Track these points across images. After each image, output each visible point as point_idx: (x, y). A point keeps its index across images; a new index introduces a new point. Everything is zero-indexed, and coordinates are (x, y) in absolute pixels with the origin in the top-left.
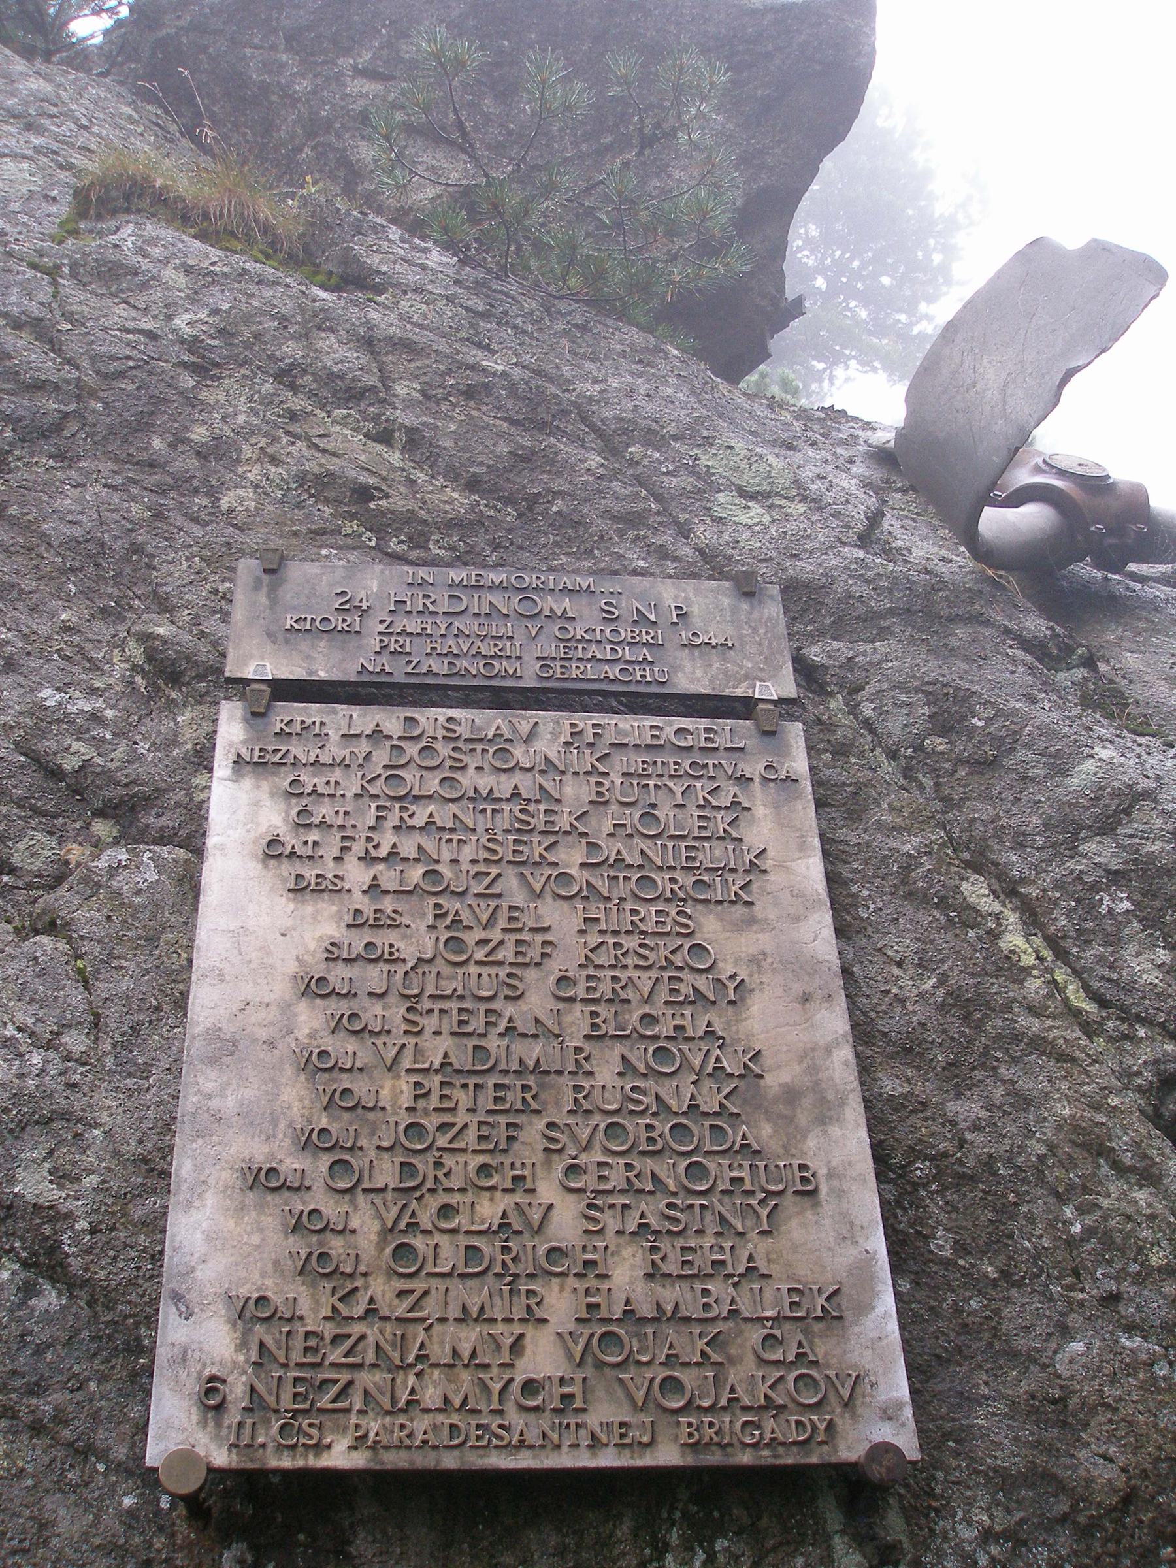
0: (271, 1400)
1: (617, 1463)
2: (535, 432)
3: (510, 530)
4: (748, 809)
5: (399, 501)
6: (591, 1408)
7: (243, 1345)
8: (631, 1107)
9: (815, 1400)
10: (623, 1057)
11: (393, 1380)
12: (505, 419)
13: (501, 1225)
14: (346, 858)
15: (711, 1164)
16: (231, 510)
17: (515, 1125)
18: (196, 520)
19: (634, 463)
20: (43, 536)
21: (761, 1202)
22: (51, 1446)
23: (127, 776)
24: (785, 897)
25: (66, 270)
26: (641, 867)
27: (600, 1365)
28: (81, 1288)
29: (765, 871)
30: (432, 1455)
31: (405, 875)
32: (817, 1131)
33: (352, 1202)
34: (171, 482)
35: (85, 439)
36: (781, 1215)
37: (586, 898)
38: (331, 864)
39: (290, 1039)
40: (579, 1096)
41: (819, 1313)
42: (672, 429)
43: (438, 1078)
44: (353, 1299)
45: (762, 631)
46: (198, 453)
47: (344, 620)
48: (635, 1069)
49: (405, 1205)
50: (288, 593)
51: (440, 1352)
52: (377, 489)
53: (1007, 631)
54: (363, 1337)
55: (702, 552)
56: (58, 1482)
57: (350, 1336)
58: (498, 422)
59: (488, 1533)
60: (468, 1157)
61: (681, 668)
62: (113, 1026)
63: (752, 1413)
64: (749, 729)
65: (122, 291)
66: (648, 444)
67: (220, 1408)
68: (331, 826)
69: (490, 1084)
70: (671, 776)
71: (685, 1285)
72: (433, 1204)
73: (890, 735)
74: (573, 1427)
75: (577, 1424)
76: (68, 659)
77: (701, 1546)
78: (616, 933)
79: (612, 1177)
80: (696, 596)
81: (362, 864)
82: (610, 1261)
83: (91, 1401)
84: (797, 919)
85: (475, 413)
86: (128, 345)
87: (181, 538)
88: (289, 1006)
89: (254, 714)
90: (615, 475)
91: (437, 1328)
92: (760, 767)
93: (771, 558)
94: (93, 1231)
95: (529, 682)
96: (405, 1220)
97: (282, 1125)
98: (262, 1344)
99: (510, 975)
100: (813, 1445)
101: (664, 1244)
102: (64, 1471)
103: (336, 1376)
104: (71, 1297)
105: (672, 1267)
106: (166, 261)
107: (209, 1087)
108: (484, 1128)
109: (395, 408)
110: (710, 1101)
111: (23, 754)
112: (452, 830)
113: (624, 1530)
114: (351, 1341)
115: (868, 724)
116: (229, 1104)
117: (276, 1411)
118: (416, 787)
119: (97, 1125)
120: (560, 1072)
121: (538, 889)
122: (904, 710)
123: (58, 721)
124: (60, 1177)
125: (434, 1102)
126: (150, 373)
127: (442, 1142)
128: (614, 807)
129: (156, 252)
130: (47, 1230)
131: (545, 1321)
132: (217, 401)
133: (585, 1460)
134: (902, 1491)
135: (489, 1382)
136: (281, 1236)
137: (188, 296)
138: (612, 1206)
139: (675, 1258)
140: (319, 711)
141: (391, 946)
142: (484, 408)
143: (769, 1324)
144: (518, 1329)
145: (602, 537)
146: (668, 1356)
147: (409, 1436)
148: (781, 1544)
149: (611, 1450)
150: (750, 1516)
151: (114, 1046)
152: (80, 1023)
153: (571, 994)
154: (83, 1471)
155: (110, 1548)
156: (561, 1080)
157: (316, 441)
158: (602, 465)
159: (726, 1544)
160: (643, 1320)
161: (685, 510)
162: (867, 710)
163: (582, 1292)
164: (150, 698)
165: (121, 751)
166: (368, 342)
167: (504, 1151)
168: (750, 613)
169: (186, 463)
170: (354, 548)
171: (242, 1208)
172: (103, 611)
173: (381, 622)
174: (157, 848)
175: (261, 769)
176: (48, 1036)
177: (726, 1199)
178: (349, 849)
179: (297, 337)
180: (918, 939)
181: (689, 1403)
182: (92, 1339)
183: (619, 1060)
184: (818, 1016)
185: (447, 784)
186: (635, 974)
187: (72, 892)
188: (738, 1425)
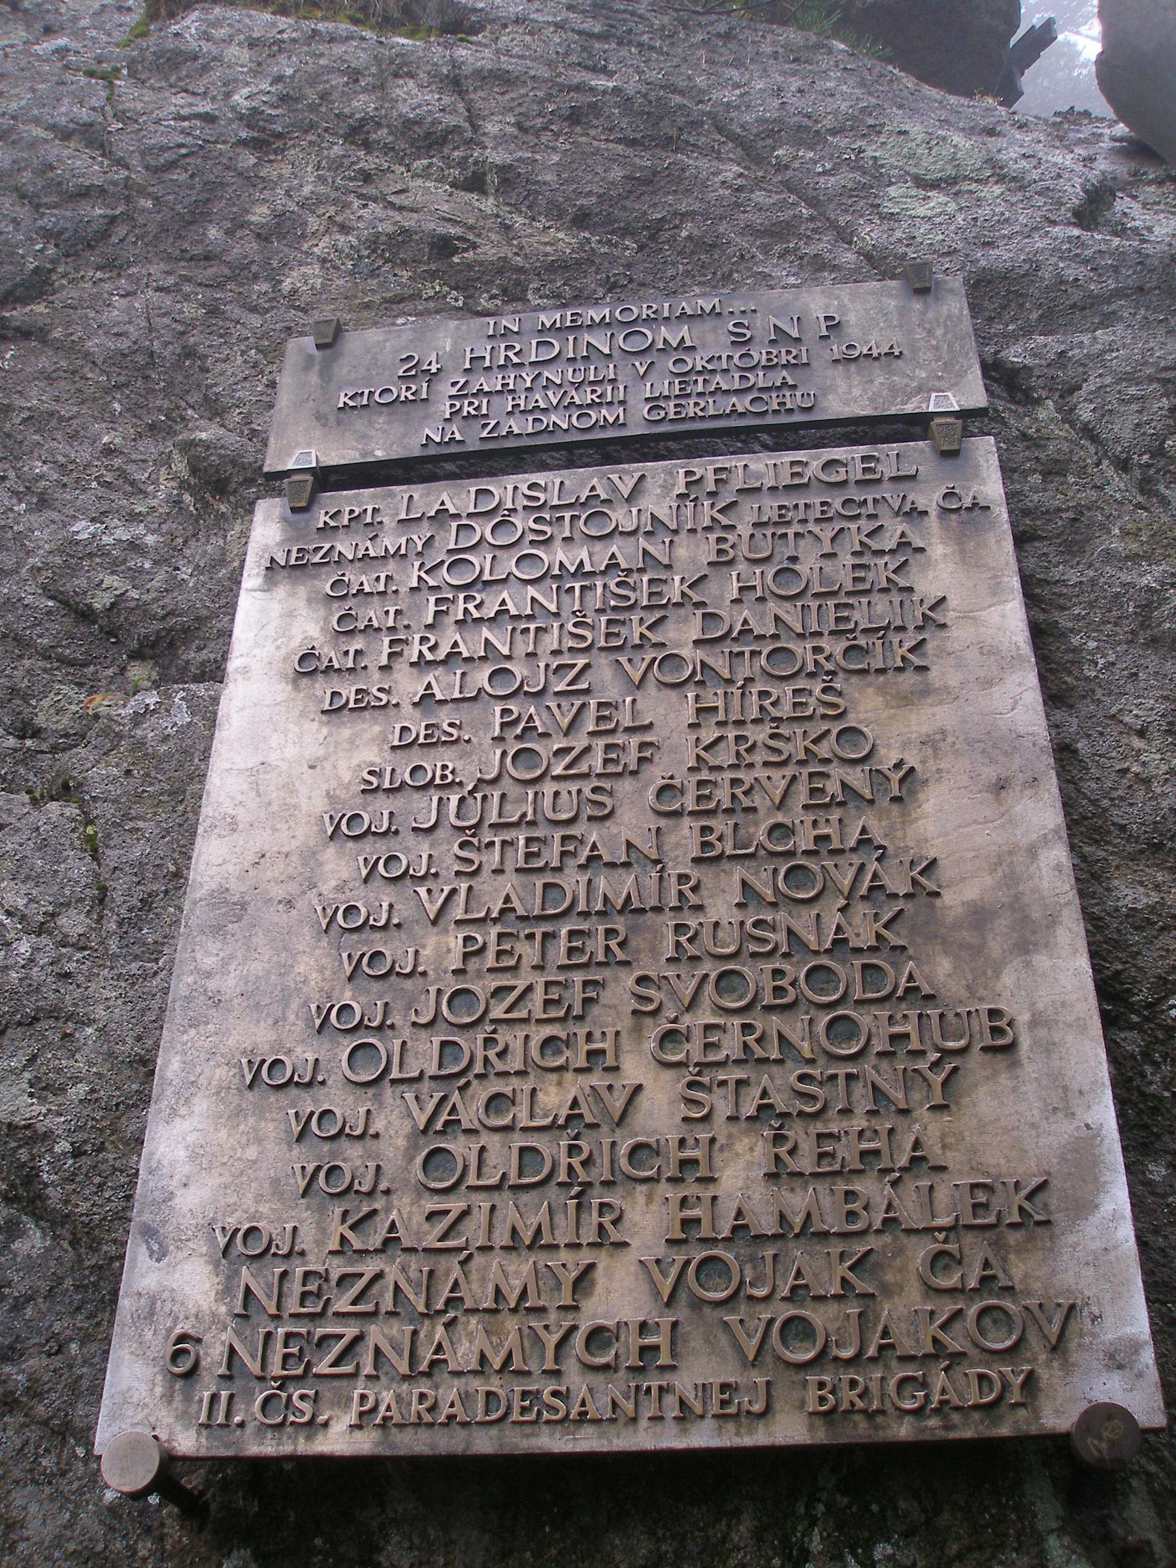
0: (255, 1367)
1: (715, 1443)
2: (658, 151)
3: (629, 266)
4: (921, 550)
5: (490, 250)
6: (682, 1364)
7: (226, 1291)
8: (753, 947)
9: (1008, 1343)
10: (744, 883)
11: (415, 1333)
12: (619, 141)
13: (569, 1118)
14: (396, 666)
15: (864, 1019)
16: (294, 292)
17: (595, 983)
18: (254, 309)
19: (781, 167)
20: (87, 354)
21: (935, 1065)
22: (25, 1425)
23: (163, 607)
24: (972, 656)
25: (125, 72)
26: (775, 637)
27: (698, 1304)
28: (63, 1225)
29: (944, 626)
30: (461, 1434)
31: (468, 678)
32: (1017, 963)
33: (377, 1098)
34: (227, 271)
35: (135, 243)
36: (964, 1081)
37: (701, 683)
38: (377, 675)
39: (312, 896)
40: (683, 939)
41: (1016, 1218)
42: (828, 122)
43: (494, 931)
44: (368, 1226)
45: (939, 332)
46: (259, 235)
47: (408, 389)
48: (760, 897)
49: (444, 1099)
50: (343, 369)
51: (479, 1293)
52: (460, 239)
54: (379, 1276)
55: (868, 257)
56: (31, 1471)
57: (361, 1275)
58: (611, 146)
59: (557, 1536)
60: (532, 1029)
61: (832, 389)
62: (119, 900)
63: (914, 1366)
64: (922, 451)
65: (180, 79)
66: (799, 143)
67: (191, 1374)
68: (379, 629)
69: (564, 932)
70: (817, 520)
71: (822, 1187)
72: (481, 1093)
73: (1117, 440)
74: (654, 1392)
75: (661, 1388)
76: (107, 485)
77: (855, 1555)
78: (740, 723)
79: (725, 1043)
81: (414, 671)
82: (718, 1158)
83: (71, 1367)
84: (988, 683)
85: (583, 139)
86: (182, 132)
87: (238, 331)
88: (314, 853)
89: (294, 510)
90: (758, 184)
91: (479, 1260)
92: (937, 496)
93: (955, 250)
94: (77, 1153)
95: (636, 429)
96: (444, 1117)
97: (295, 1004)
98: (248, 1291)
99: (595, 790)
100: (1003, 1408)
101: (795, 1132)
102: (37, 1456)
103: (339, 1330)
104: (55, 1237)
105: (805, 1163)
106: (229, 40)
107: (209, 962)
108: (554, 989)
109: (485, 148)
110: (862, 933)
111: (52, 598)
112: (531, 618)
113: (743, 1531)
114: (361, 1284)
115: (1088, 432)
116: (229, 984)
117: (261, 1379)
118: (487, 571)
119: (91, 1022)
120: (658, 910)
121: (636, 677)
122: (1134, 407)
123: (91, 555)
124: (42, 1089)
125: (490, 960)
126: (205, 158)
127: (498, 1012)
128: (742, 567)
129: (221, 33)
130: (23, 1155)
131: (625, 1244)
132: (280, 176)
133: (671, 1439)
134: (1152, 1468)
135: (542, 1333)
136: (285, 1147)
137: (251, 70)
138: (723, 1083)
139: (808, 1147)
140: (373, 497)
141: (444, 767)
142: (592, 132)
143: (941, 1236)
144: (585, 1257)
145: (742, 256)
146: (794, 1289)
147: (432, 1409)
148: (969, 1549)
149: (709, 1423)
150: (924, 1510)
151: (120, 924)
152: (81, 900)
153: (676, 806)
154: (59, 1457)
155: (86, 1555)
156: (659, 919)
157: (392, 198)
158: (741, 175)
159: (890, 1550)
160: (760, 1238)
161: (846, 211)
162: (1085, 413)
163: (675, 1204)
164: (199, 516)
165: (160, 578)
166: (454, 82)
167: (580, 1018)
168: (924, 313)
169: (246, 248)
170: (437, 312)
171: (238, 1113)
172: (152, 427)
173: (454, 384)
174: (193, 687)
175: (298, 573)
176: (40, 918)
177: (885, 1065)
178: (400, 654)
179: (370, 89)
180: (1166, 698)
181: (823, 1353)
182: (77, 1288)
183: (738, 887)
184: (1019, 808)
185: (525, 564)
186: (761, 773)
187: (90, 747)
188: (892, 1383)
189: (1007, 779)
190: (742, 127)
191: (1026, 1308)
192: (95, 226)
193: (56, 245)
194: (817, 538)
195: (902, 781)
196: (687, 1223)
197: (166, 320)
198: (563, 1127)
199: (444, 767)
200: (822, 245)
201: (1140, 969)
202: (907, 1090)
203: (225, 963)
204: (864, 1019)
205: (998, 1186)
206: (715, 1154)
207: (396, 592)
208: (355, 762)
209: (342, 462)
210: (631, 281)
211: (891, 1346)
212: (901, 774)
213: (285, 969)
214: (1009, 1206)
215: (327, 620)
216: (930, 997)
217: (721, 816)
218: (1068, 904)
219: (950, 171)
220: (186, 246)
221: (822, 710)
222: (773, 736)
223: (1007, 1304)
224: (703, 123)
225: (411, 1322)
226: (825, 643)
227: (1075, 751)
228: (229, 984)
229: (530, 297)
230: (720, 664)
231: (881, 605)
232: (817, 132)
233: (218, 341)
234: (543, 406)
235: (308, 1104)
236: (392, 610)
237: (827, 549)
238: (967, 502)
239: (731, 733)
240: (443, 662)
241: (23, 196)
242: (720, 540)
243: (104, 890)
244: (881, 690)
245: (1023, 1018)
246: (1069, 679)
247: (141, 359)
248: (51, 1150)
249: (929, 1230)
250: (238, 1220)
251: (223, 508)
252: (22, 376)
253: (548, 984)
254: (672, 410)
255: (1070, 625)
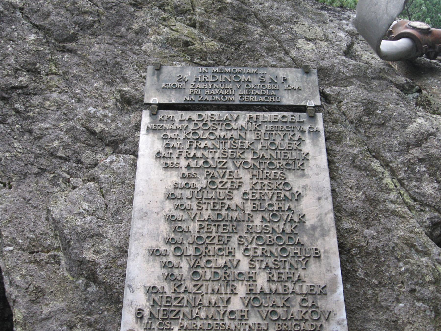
2: (241, 22)
3: (232, 54)
4: (304, 141)
5: (197, 46)
6: (250, 319)
7: (149, 300)
8: (265, 231)
10: (263, 217)
12: (231, 18)
13: (224, 266)
15: (289, 248)
18: (134, 53)
21: (303, 260)
24: (314, 168)
26: (270, 159)
27: (253, 307)
31: (198, 162)
32: (321, 238)
33: (181, 259)
36: (309, 263)
39: (163, 212)
40: (249, 228)
41: (319, 293)
42: (285, 19)
44: (180, 287)
45: (310, 84)
46: (135, 32)
48: (266, 220)
49: (196, 260)
50: (163, 76)
53: (391, 82)
54: (183, 298)
58: (229, 19)
61: (284, 97)
70: (280, 131)
73: (350, 116)
74: (244, 324)
76: (97, 98)
78: (262, 179)
80: (290, 73)
93: (315, 60)
94: (106, 268)
96: (196, 264)
97: (161, 237)
105: (275, 279)
107: (139, 226)
109: (196, 16)
110: (288, 229)
111: (84, 127)
112: (212, 149)
115: (344, 113)
116: (145, 231)
117: (158, 319)
118: (202, 135)
119: (107, 238)
122: (355, 108)
123: (94, 117)
127: (208, 241)
130: (92, 268)
135: (220, 311)
136: (160, 269)
138: (258, 261)
140: (172, 113)
142: (224, 15)
143: (304, 295)
144: (229, 296)
146: (273, 305)
151: (112, 214)
157: (172, 27)
158: (262, 32)
165: (114, 125)
167: (226, 244)
168: (307, 78)
169: (131, 35)
173: (192, 85)
174: (124, 155)
177: (293, 259)
183: (261, 217)
188: (293, 325)
189: (321, 197)
190: (262, 17)
191: (321, 311)
192: (89, 23)
193: (79, 27)
194: (280, 135)
195: (298, 196)
196: (251, 290)
197: (110, 53)
198: (223, 268)
199: (193, 184)
200: (282, 55)
201: (347, 242)
202: (297, 264)
203: (144, 226)
204: (289, 248)
205: (316, 286)
206: (256, 276)
207: (179, 139)
208: (172, 180)
209: (164, 102)
210: (233, 58)
211: (293, 317)
212: (298, 194)
213: (158, 229)
214: (317, 290)
215: (163, 144)
216: (303, 245)
217: (257, 201)
218: (333, 226)
219: (314, 37)
220: (115, 32)
221: (280, 178)
222: (269, 183)
223: (317, 310)
224: (252, 15)
225: (191, 308)
226: (281, 161)
227: (335, 191)
228: (145, 231)
229: (208, 60)
230: (257, 164)
231: (294, 154)
232: (282, 22)
233: (125, 61)
234: (214, 93)
235: (164, 260)
236: (179, 143)
237: (282, 138)
238: (315, 130)
239: (260, 181)
240: (192, 158)
241: (67, 10)
242: (257, 134)
243: (107, 205)
244: (294, 174)
245: (322, 251)
246: (335, 174)
247: (104, 63)
248: (100, 267)
249: (301, 294)
250: (150, 284)
251: (129, 108)
252: (70, 63)
253: (219, 236)
254: (246, 98)
255: (336, 161)
